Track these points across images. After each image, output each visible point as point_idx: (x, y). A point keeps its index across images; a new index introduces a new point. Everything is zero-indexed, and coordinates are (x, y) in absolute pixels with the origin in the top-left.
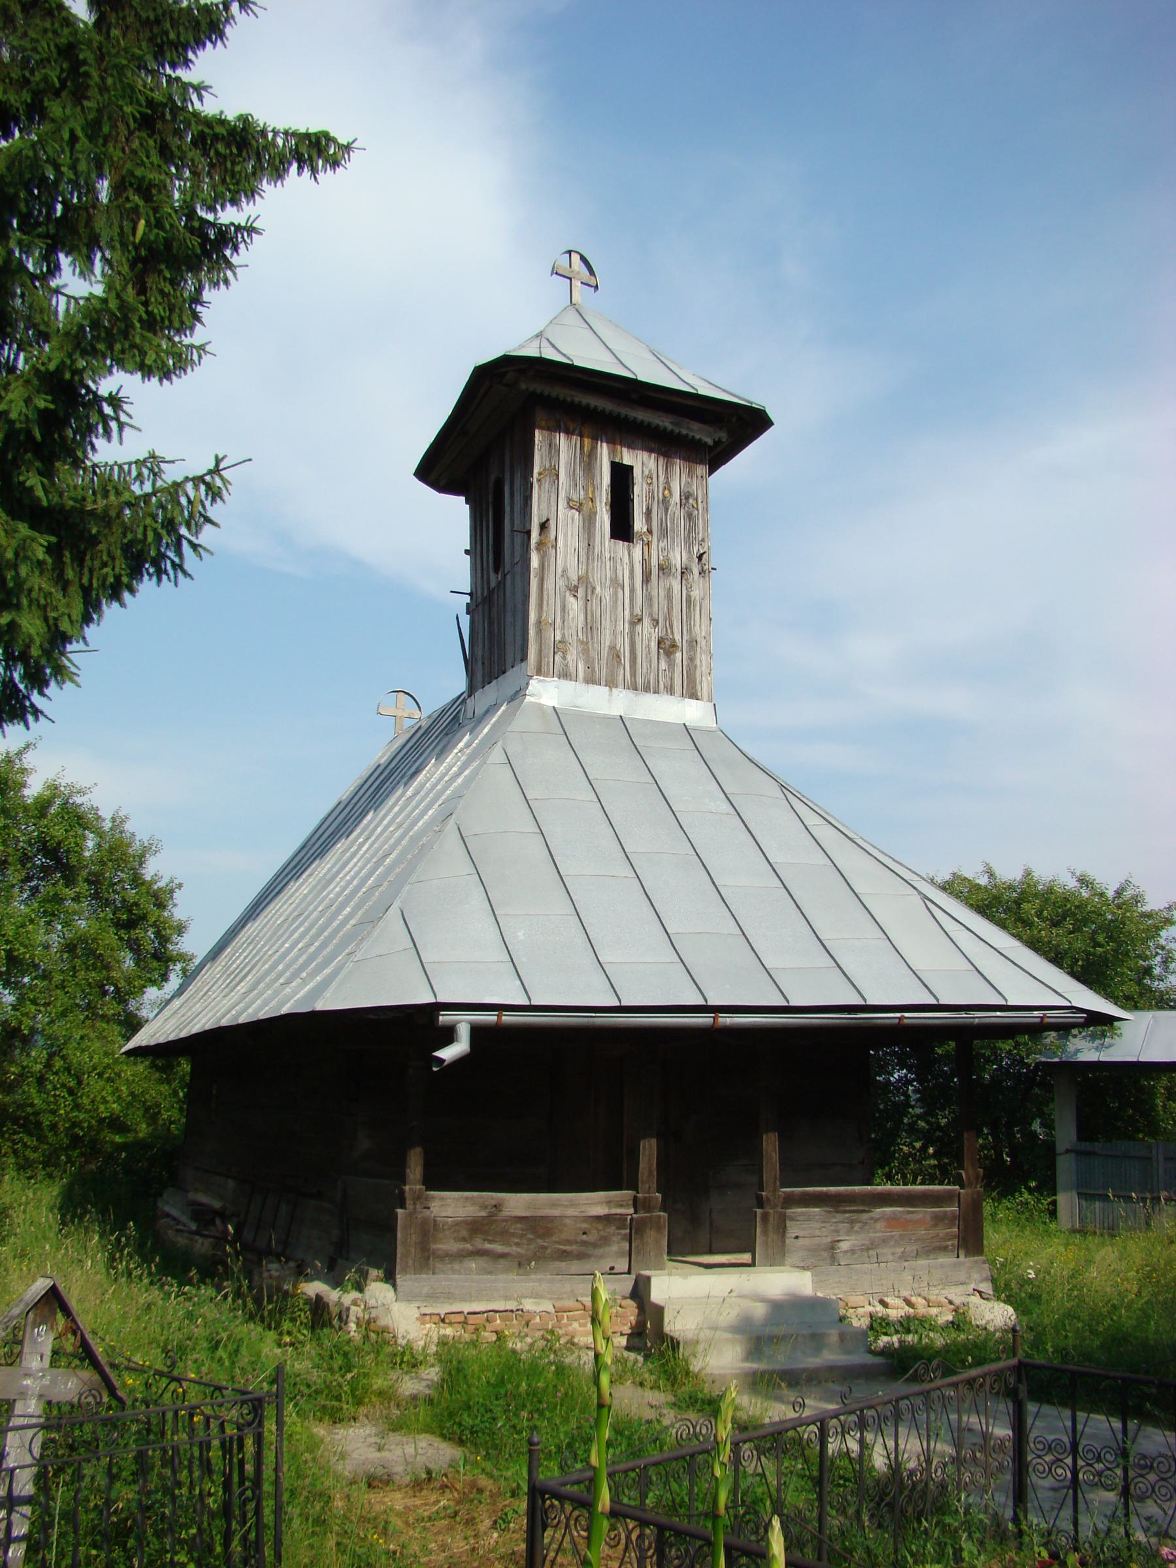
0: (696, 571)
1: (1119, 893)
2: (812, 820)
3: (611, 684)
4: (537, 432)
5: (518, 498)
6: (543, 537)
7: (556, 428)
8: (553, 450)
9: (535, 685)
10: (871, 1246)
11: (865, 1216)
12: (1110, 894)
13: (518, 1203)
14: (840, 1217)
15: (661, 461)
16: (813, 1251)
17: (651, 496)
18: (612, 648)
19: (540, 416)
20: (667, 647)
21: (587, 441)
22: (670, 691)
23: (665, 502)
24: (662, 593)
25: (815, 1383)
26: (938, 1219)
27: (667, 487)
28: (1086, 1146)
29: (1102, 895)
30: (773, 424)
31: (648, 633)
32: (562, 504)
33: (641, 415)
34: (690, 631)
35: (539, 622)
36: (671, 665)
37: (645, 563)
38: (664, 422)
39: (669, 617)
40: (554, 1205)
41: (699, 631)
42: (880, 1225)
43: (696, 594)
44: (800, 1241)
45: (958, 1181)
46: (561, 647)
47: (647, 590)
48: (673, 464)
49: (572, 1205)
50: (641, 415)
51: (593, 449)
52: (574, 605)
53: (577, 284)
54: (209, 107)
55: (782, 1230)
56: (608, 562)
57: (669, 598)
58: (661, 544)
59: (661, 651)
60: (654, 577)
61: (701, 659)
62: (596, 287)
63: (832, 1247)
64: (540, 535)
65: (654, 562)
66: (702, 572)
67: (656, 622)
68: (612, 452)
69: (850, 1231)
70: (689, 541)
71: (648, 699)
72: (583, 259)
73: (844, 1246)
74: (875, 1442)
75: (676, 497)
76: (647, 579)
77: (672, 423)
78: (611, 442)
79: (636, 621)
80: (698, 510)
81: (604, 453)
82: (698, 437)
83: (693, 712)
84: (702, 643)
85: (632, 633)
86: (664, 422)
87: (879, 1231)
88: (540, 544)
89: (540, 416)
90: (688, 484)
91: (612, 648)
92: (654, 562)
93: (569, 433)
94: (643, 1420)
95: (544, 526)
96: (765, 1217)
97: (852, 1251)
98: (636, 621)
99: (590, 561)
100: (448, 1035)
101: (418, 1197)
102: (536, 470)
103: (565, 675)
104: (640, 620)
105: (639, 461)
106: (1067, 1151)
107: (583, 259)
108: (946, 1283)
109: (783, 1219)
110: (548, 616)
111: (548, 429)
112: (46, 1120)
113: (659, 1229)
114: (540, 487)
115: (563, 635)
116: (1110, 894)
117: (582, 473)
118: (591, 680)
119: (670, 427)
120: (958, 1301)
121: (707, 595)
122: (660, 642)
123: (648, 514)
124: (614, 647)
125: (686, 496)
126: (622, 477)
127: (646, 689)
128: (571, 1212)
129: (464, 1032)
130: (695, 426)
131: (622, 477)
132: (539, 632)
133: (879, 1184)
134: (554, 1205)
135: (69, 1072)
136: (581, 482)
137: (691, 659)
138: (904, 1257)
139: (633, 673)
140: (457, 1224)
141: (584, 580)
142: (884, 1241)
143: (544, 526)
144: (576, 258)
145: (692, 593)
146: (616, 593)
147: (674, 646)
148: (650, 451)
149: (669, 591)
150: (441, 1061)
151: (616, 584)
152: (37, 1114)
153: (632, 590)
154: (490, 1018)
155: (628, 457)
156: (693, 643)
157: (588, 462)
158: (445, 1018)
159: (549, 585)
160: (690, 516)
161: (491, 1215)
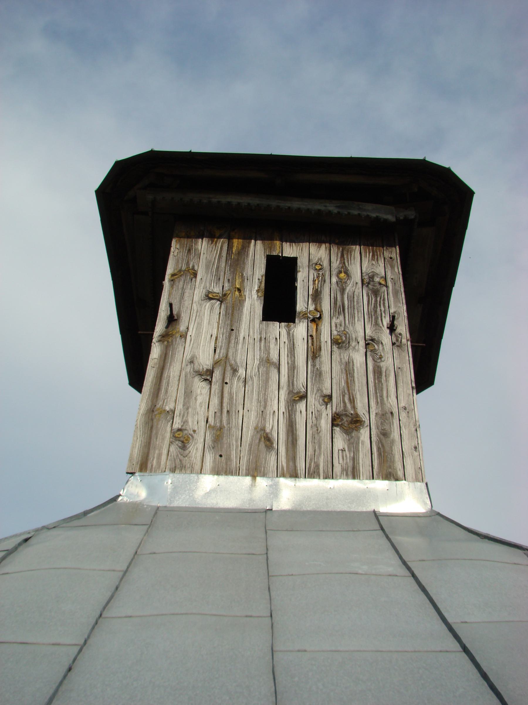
4: (174, 242)
6: (170, 329)
15: (334, 249)
24: (336, 368)
25: (215, 440)
30: (449, 167)
34: (381, 402)
47: (314, 365)
48: (350, 252)
56: (257, 344)
58: (334, 320)
59: (337, 429)
64: (167, 327)
74: (198, 269)
77: (337, 207)
80: (387, 287)
82: (374, 215)
88: (164, 337)
99: (232, 345)
102: (170, 271)
104: (304, 397)
114: (172, 286)
115: (185, 422)
117: (228, 268)
119: (335, 210)
124: (263, 429)
133: (380, 398)
143: (172, 320)
145: (382, 364)
153: (292, 368)
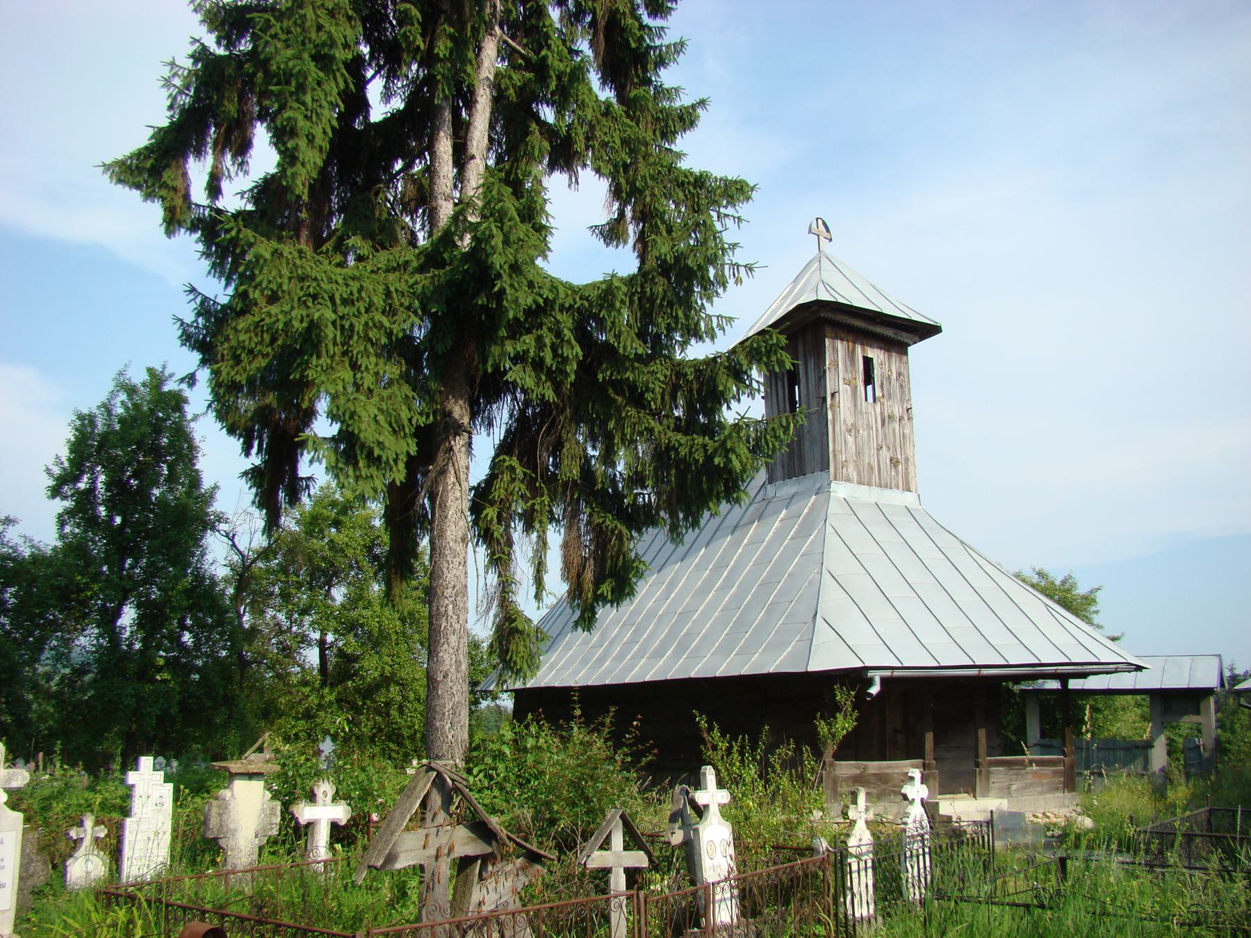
0: (906, 418)
1: (1064, 582)
2: (982, 562)
3: (869, 484)
5: (812, 375)
7: (835, 337)
8: (835, 350)
9: (834, 486)
10: (1026, 787)
11: (1023, 771)
12: (1057, 583)
13: (874, 766)
14: (1012, 772)
16: (1001, 789)
17: (882, 376)
18: (869, 464)
19: (828, 331)
20: (894, 462)
21: (851, 344)
22: (898, 487)
23: (889, 378)
26: (1055, 773)
27: (890, 370)
28: (1044, 742)
29: (1053, 583)
31: (886, 455)
32: (841, 382)
33: (879, 330)
35: (834, 451)
36: (897, 472)
37: (882, 414)
38: (889, 333)
39: (894, 446)
40: (889, 767)
41: (909, 453)
42: (1029, 776)
43: (907, 431)
44: (996, 785)
45: (1064, 754)
46: (844, 465)
49: (897, 767)
50: (879, 330)
51: (854, 349)
52: (850, 439)
53: (821, 238)
54: (683, 165)
55: (988, 778)
57: (894, 434)
60: (886, 423)
61: (911, 469)
62: (831, 240)
63: (1009, 788)
65: (886, 414)
66: (909, 419)
67: (889, 448)
68: (863, 350)
69: (1016, 780)
70: (902, 401)
71: (887, 492)
72: (824, 223)
73: (1014, 787)
75: (894, 376)
76: (883, 425)
78: (862, 344)
79: (879, 448)
81: (859, 349)
83: (908, 499)
84: (911, 459)
85: (878, 455)
86: (889, 333)
87: (1029, 779)
88: (832, 405)
89: (828, 331)
90: (900, 367)
91: (869, 464)
92: (886, 414)
93: (842, 340)
94: (1160, 805)
95: (833, 395)
96: (980, 772)
97: (1017, 790)
98: (879, 448)
100: (870, 682)
101: (831, 765)
102: (827, 363)
103: (848, 480)
105: (876, 354)
106: (1035, 745)
107: (824, 223)
108: (1063, 806)
109: (988, 773)
110: (838, 447)
111: (832, 338)
112: (406, 732)
113: (934, 778)
116: (1057, 583)
118: (860, 483)
120: (1068, 815)
121: (912, 432)
122: (891, 460)
123: (882, 385)
125: (899, 374)
126: (868, 362)
127: (886, 487)
128: (896, 771)
129: (877, 680)
130: (905, 334)
131: (868, 362)
132: (835, 456)
134: (889, 767)
135: (419, 701)
136: (849, 369)
137: (907, 469)
138: (1041, 793)
139: (880, 479)
140: (848, 778)
141: (854, 425)
142: (1032, 784)
143: (833, 395)
144: (820, 221)
146: (869, 433)
147: (898, 462)
148: (881, 349)
149: (894, 430)
150: (870, 695)
151: (869, 427)
152: (399, 729)
154: (887, 673)
155: (871, 353)
156: (907, 459)
157: (851, 355)
158: (870, 674)
159: (837, 429)
160: (901, 386)
161: (862, 773)
